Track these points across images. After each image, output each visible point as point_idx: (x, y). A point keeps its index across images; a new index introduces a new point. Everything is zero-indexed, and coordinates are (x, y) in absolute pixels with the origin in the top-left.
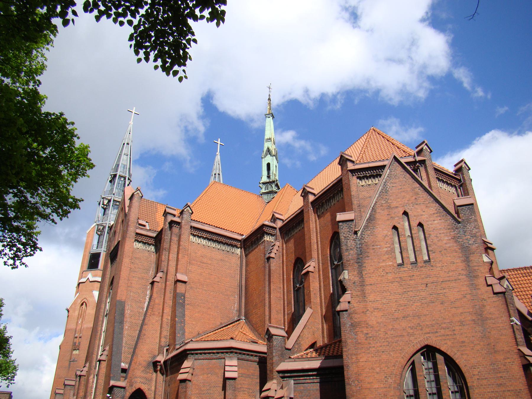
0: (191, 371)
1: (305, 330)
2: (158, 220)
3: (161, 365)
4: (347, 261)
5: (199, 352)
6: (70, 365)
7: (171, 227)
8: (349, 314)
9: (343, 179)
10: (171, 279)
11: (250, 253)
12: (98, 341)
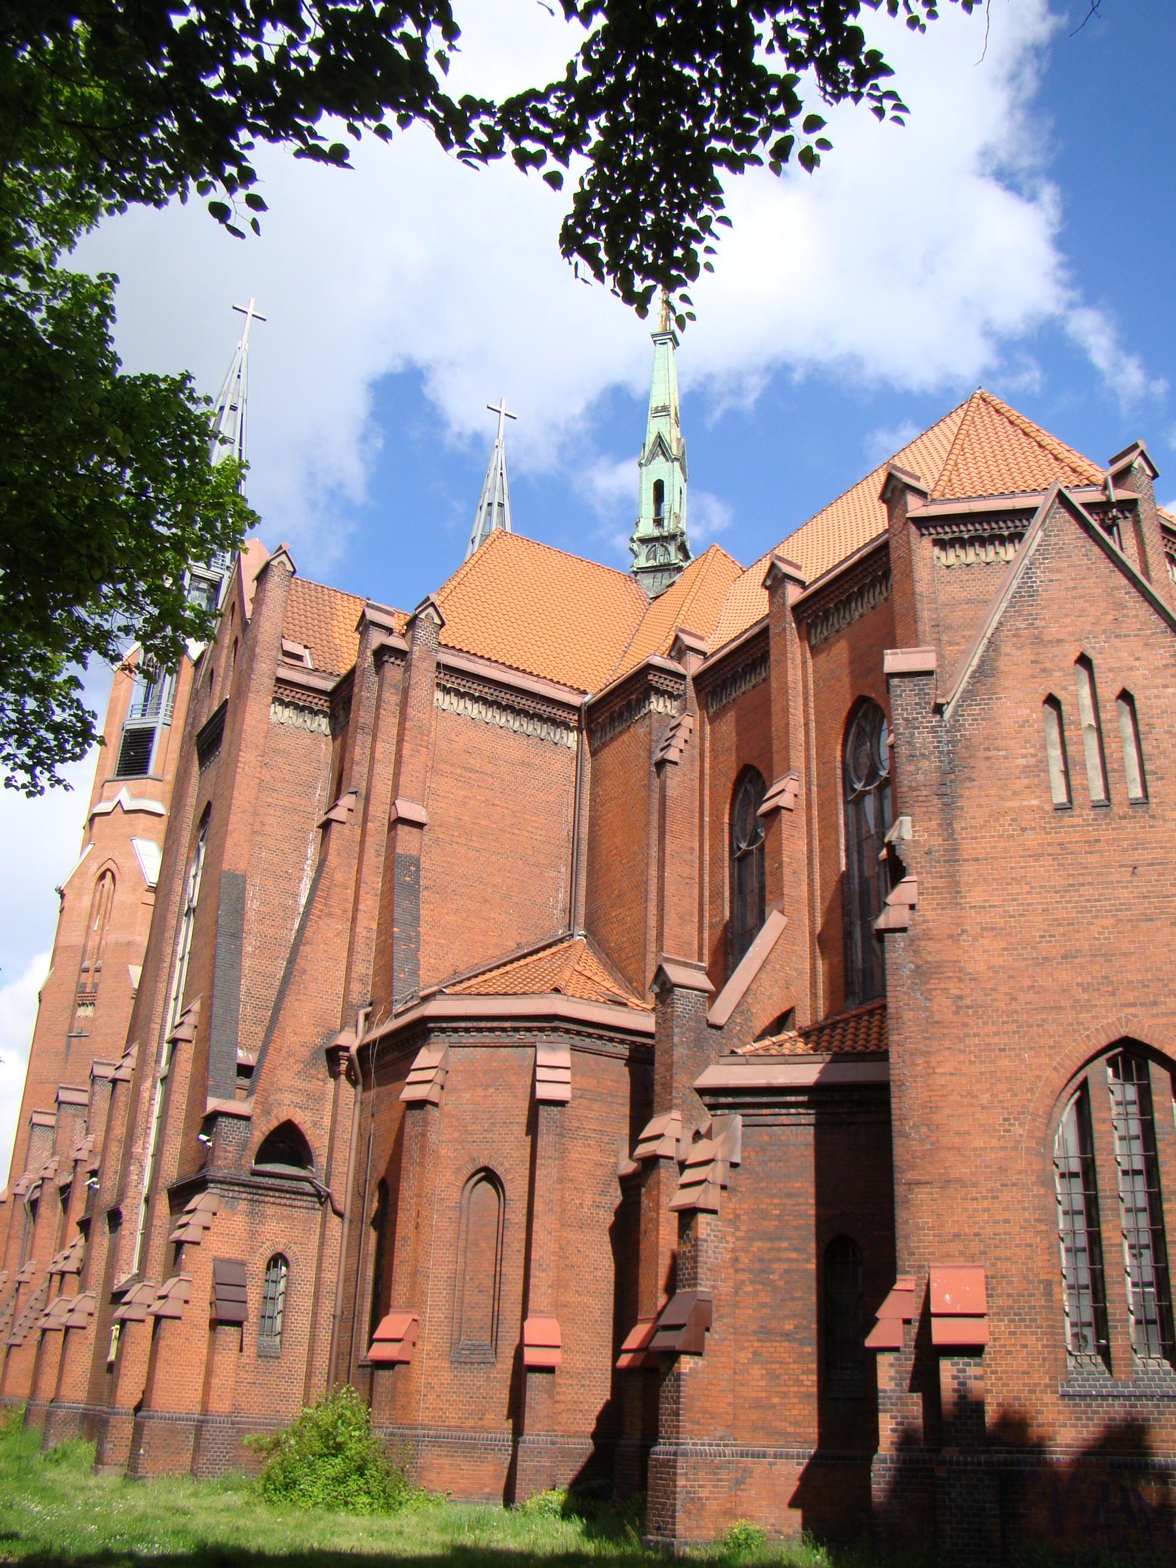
0: (439, 1079)
1: (763, 975)
2: (337, 641)
3: (350, 1059)
4: (911, 788)
5: (463, 1024)
6: (68, 1046)
7: (379, 664)
8: (912, 940)
9: (893, 544)
10: (380, 814)
11: (604, 745)
12: (165, 984)
